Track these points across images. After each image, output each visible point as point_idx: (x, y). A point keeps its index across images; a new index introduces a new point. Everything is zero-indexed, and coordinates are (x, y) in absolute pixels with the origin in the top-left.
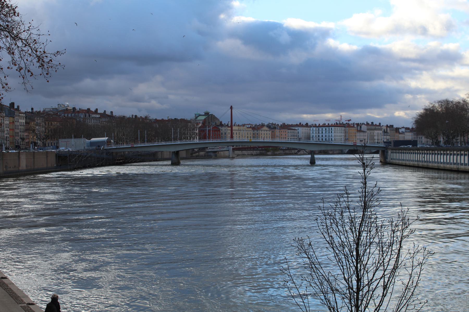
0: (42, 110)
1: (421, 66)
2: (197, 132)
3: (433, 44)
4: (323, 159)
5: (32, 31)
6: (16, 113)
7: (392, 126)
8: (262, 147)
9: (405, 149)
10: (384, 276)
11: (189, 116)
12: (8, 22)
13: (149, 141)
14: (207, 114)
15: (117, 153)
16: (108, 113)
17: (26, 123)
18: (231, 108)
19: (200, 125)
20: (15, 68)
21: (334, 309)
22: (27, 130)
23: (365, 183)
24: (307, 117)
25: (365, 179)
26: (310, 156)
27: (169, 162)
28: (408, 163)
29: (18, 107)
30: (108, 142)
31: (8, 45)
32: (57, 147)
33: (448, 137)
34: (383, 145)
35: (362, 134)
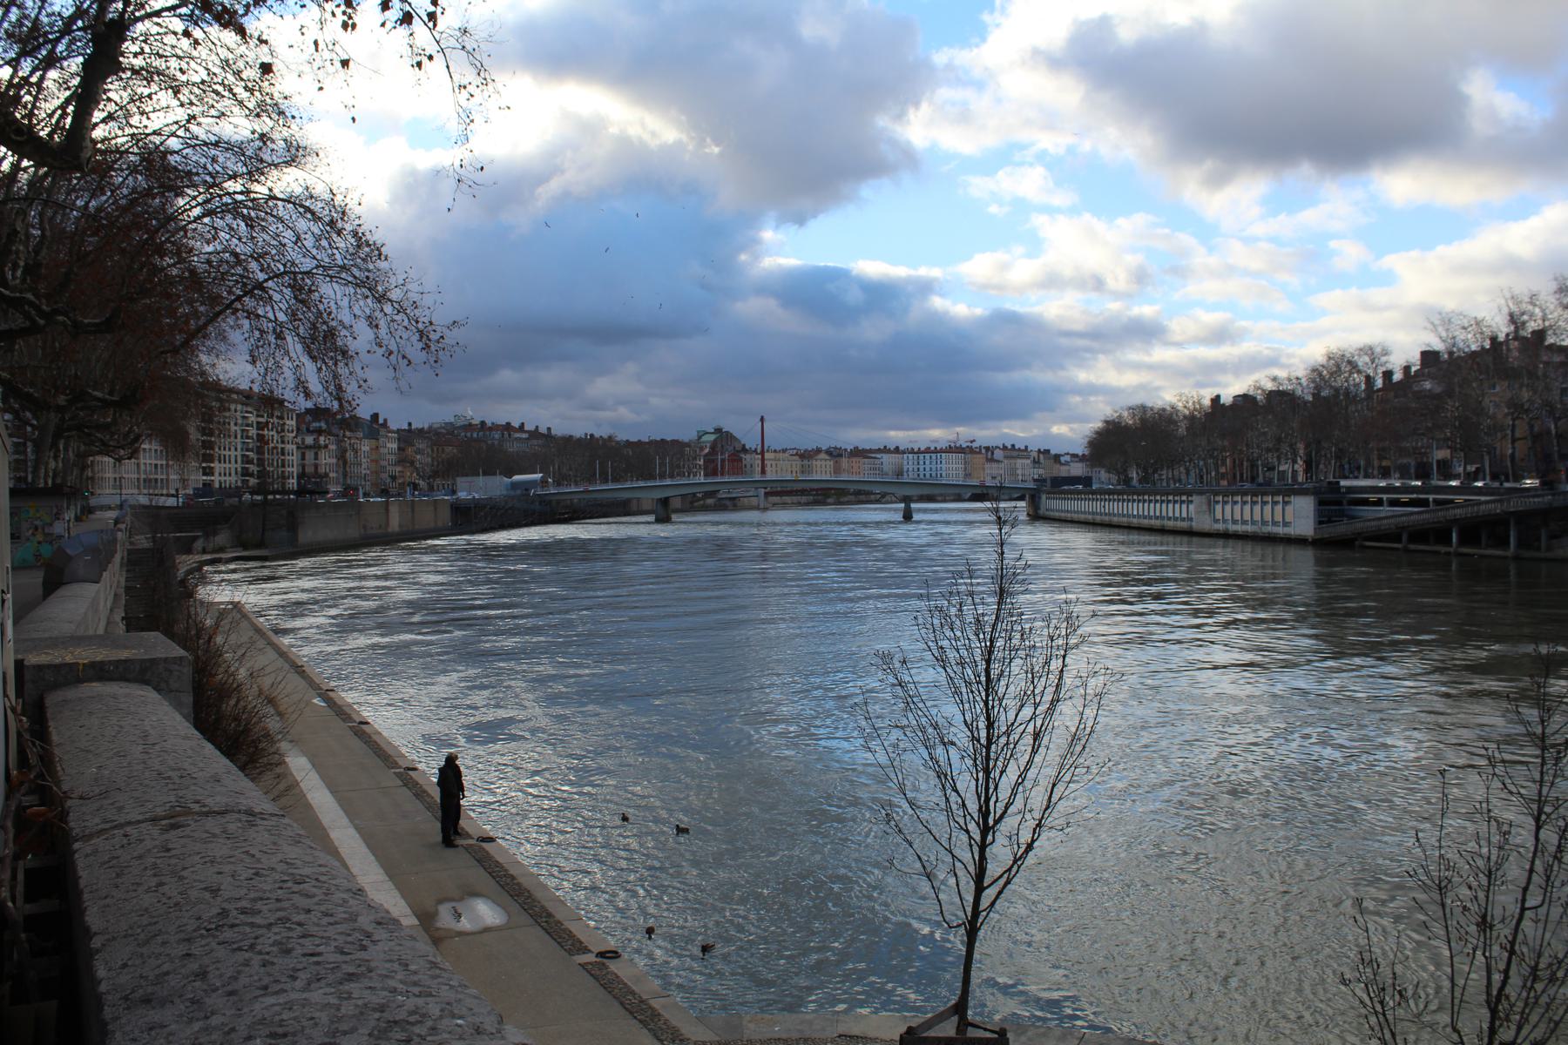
0: (426, 426)
1: (1095, 345)
2: (702, 462)
3: (1114, 306)
4: (925, 511)
5: (409, 286)
6: (383, 432)
7: (1047, 452)
8: (817, 490)
9: (1071, 492)
10: (1034, 717)
11: (687, 435)
12: (369, 271)
13: (615, 480)
14: (718, 431)
15: (558, 502)
16: (543, 430)
17: (399, 449)
18: (762, 419)
19: (707, 450)
20: (381, 351)
21: (946, 775)
22: (400, 462)
23: (1003, 553)
24: (896, 437)
25: (1002, 545)
26: (903, 505)
27: (652, 518)
28: (1075, 516)
29: (385, 420)
30: (544, 482)
31: (368, 312)
32: (454, 492)
33: (1145, 470)
34: (1032, 485)
35: (995, 465)
